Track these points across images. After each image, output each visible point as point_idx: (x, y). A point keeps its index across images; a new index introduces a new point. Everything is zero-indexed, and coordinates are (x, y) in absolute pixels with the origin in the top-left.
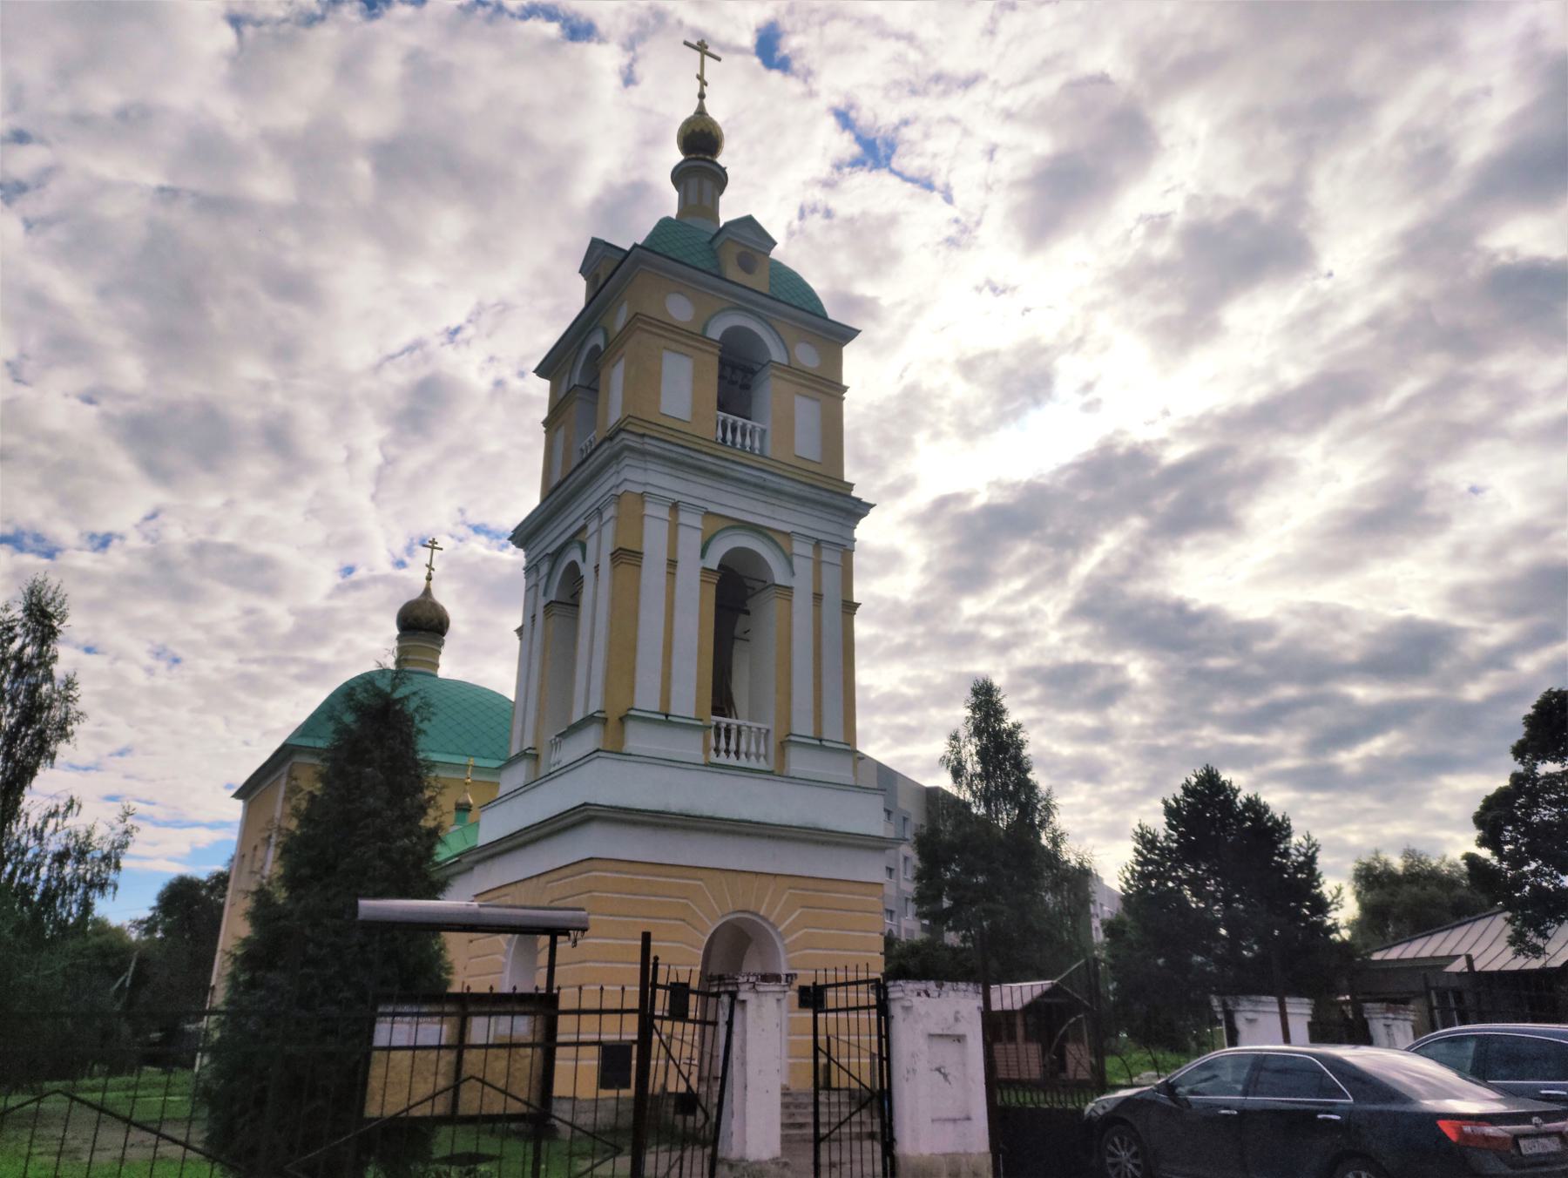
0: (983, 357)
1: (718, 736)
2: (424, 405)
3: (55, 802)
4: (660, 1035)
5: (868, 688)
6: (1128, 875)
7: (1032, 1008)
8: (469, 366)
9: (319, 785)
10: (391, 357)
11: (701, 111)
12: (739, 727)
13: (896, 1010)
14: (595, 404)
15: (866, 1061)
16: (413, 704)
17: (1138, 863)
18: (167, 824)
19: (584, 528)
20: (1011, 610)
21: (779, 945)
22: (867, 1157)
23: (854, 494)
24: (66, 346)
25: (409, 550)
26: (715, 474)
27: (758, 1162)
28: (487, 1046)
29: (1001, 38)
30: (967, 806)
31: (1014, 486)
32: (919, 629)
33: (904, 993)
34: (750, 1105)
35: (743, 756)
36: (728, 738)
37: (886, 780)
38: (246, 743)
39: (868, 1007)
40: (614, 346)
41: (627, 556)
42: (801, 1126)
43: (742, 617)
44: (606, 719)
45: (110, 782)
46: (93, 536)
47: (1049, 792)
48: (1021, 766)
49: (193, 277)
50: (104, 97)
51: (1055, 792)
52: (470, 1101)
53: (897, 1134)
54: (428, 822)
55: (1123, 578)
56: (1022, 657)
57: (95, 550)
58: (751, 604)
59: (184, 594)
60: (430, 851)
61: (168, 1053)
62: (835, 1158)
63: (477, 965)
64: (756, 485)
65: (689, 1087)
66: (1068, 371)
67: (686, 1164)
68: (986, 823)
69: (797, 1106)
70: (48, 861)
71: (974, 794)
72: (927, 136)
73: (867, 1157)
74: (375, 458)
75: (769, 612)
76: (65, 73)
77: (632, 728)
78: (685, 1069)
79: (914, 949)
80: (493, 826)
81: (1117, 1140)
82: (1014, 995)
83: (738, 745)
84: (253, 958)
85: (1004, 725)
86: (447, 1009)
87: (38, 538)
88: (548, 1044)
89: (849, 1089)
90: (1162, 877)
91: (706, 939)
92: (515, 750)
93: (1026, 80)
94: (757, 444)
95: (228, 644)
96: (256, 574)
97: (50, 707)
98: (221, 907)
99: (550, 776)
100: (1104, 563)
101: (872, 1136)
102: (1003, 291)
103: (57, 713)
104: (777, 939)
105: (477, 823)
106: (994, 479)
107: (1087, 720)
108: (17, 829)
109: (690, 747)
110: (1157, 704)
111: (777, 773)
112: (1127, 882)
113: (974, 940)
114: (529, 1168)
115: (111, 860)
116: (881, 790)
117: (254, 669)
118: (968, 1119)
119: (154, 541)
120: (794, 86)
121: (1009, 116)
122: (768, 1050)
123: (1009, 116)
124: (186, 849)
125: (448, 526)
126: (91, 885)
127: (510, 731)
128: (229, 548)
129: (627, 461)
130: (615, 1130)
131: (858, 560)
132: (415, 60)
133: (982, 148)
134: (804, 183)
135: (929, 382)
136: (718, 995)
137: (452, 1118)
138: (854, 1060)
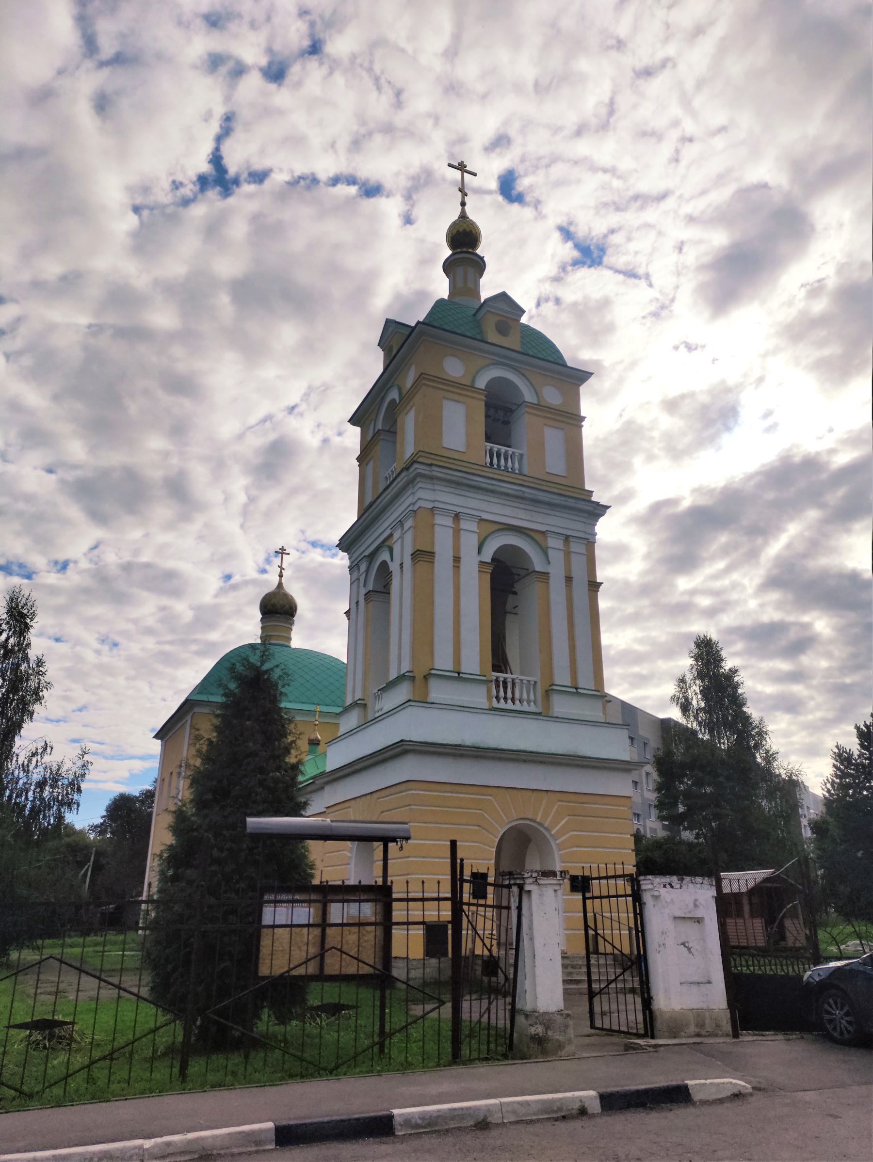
0: (683, 397)
1: (498, 686)
2: (275, 460)
3: (35, 745)
4: (467, 917)
5: (609, 647)
6: (829, 786)
7: (756, 891)
8: (305, 431)
9: (215, 734)
10: (251, 427)
11: (463, 216)
12: (513, 680)
13: (647, 898)
14: (395, 442)
15: (625, 932)
16: (277, 673)
17: (836, 776)
18: (112, 758)
19: (391, 535)
20: (717, 584)
21: (553, 844)
22: (631, 1007)
23: (594, 498)
24: (34, 436)
25: (268, 561)
26: (487, 490)
27: (546, 1013)
28: (342, 925)
29: (683, 163)
30: (694, 733)
31: (712, 491)
32: (645, 602)
33: (652, 885)
34: (539, 971)
35: (517, 702)
36: (505, 689)
37: (629, 715)
38: (164, 700)
39: (626, 896)
40: (406, 398)
41: (423, 556)
42: (578, 982)
43: (511, 597)
44: (414, 677)
45: (73, 730)
46: (56, 563)
47: (761, 721)
48: (738, 702)
49: (116, 382)
50: (51, 268)
51: (765, 720)
52: (333, 965)
53: (653, 993)
54: (292, 759)
55: (805, 556)
56: (727, 620)
57: (59, 571)
58: (517, 587)
59: (119, 599)
60: (294, 778)
61: (118, 920)
62: (606, 1008)
63: (333, 863)
64: (517, 497)
65: (491, 955)
66: (750, 405)
67: (493, 1010)
68: (710, 746)
69: (573, 967)
70: (33, 787)
71: (700, 724)
72: (629, 239)
73: (631, 1007)
74: (242, 498)
75: (531, 591)
76: (27, 254)
77: (433, 683)
78: (487, 942)
79: (658, 844)
80: (336, 757)
81: (831, 1001)
82: (740, 880)
83: (513, 693)
84: (177, 860)
85: (722, 671)
86: (313, 897)
87: (21, 566)
88: (386, 924)
89: (613, 954)
90: (858, 787)
91: (497, 840)
92: (349, 701)
93: (704, 192)
94: (517, 466)
95: (149, 631)
96: (167, 582)
97: (27, 680)
98: (151, 814)
99: (375, 720)
100: (789, 546)
101: (633, 991)
102: (696, 349)
103: (33, 684)
104: (551, 840)
105: (325, 754)
106: (696, 485)
107: (784, 666)
108: (12, 765)
109: (478, 696)
110: (840, 652)
111: (544, 714)
112: (829, 791)
113: (705, 837)
114: (377, 1012)
115: (75, 786)
116: (625, 725)
117: (167, 648)
118: (709, 982)
119: (96, 564)
120: (527, 212)
121: (691, 219)
122: (549, 925)
123: (691, 219)
124: (126, 774)
125: (294, 543)
126: (62, 804)
127: (345, 685)
128: (147, 566)
129: (420, 485)
130: (438, 983)
131: (598, 553)
132: (256, 219)
133: (672, 247)
134: (540, 281)
135: (643, 419)
136: (509, 886)
137: (321, 977)
138: (616, 932)
